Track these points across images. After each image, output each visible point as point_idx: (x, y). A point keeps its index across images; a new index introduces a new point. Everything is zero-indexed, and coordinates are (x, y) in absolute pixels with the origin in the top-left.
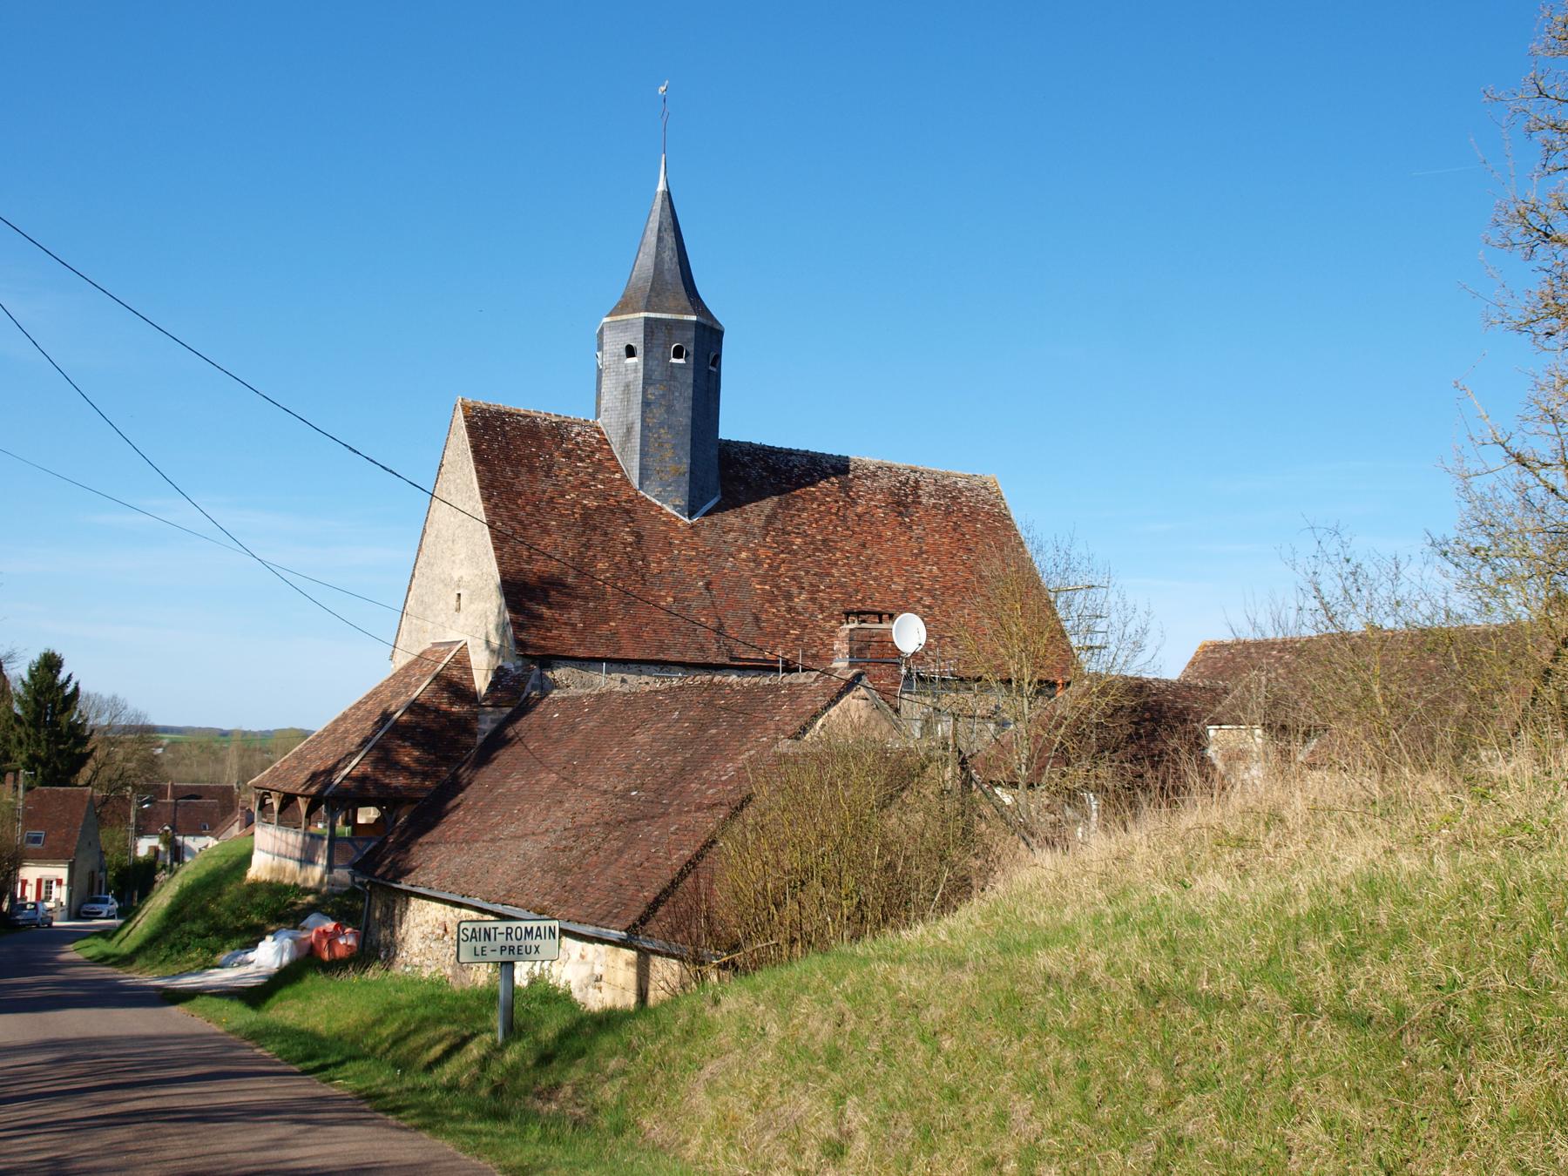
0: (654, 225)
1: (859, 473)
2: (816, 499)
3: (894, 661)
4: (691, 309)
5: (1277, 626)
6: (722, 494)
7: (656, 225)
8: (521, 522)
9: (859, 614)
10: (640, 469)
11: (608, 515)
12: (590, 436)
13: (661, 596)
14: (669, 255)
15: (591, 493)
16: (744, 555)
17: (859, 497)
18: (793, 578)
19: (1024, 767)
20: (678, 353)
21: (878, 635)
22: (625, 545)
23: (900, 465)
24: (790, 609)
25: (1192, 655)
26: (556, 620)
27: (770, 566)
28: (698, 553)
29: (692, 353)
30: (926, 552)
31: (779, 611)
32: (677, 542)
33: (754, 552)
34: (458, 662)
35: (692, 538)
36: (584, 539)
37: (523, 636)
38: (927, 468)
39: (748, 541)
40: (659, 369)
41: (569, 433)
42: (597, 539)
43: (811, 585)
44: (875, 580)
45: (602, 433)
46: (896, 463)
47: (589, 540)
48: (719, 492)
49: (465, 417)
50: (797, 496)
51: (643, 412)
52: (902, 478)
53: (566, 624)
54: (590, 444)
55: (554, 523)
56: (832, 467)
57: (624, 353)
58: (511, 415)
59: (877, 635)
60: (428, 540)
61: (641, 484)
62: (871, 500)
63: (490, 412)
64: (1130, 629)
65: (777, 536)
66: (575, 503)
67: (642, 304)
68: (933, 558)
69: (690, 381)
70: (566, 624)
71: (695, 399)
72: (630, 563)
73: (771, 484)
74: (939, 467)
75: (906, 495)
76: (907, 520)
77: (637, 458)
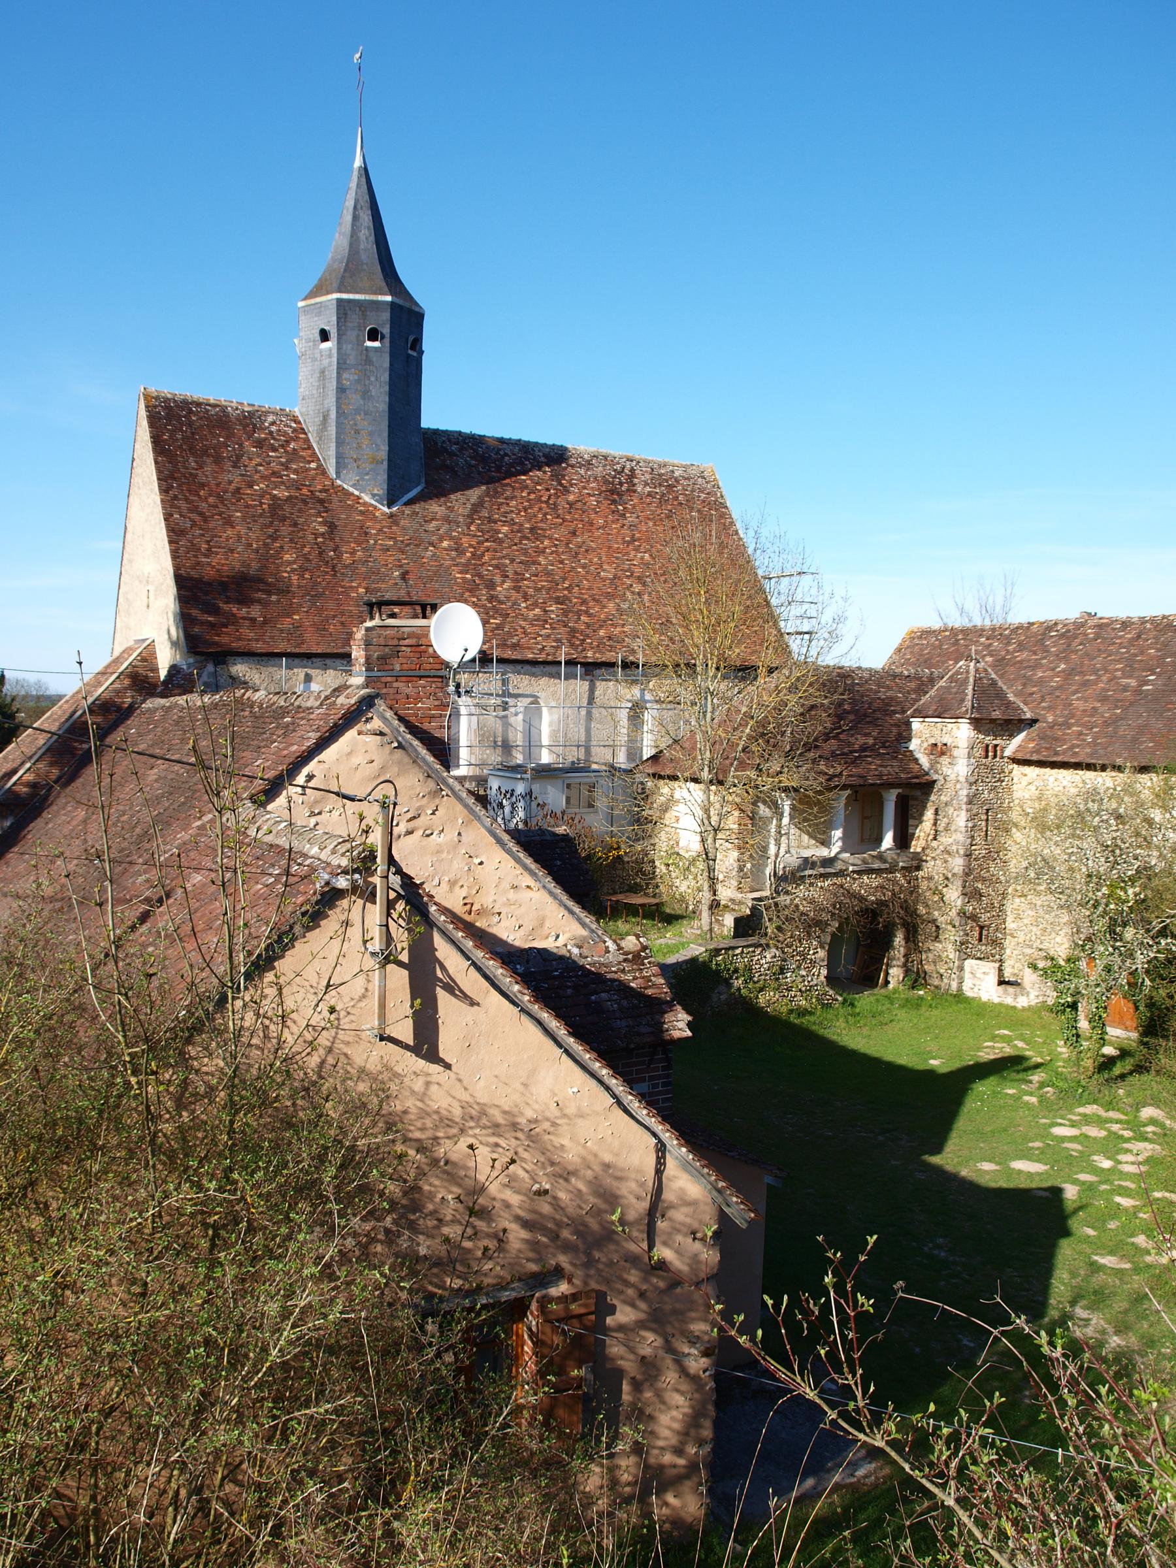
0: (350, 203)
4: (386, 289)
5: (984, 612)
6: (426, 482)
7: (352, 203)
8: (201, 514)
9: (381, 604)
10: (337, 458)
11: (300, 505)
12: (287, 426)
13: (351, 587)
15: (282, 483)
16: (445, 544)
17: (572, 485)
18: (497, 567)
19: (706, 769)
20: (373, 335)
22: (316, 536)
24: (491, 599)
25: (899, 641)
27: (473, 554)
28: (396, 542)
29: (388, 336)
30: (639, 540)
31: (479, 600)
33: (457, 540)
34: (144, 660)
35: (390, 527)
36: (271, 530)
38: (643, 457)
39: (451, 530)
40: (354, 353)
42: (285, 530)
43: (516, 573)
44: (583, 568)
45: (300, 423)
46: (612, 452)
47: (276, 531)
48: (423, 480)
49: (147, 407)
50: (506, 485)
51: (338, 399)
52: (618, 467)
54: (285, 434)
55: (239, 514)
57: (318, 338)
58: (199, 404)
59: (410, 635)
61: (338, 473)
62: (584, 488)
63: (175, 401)
65: (482, 524)
66: (263, 494)
67: (335, 285)
69: (387, 364)
72: (320, 553)
73: (479, 473)
75: (621, 484)
77: (333, 445)
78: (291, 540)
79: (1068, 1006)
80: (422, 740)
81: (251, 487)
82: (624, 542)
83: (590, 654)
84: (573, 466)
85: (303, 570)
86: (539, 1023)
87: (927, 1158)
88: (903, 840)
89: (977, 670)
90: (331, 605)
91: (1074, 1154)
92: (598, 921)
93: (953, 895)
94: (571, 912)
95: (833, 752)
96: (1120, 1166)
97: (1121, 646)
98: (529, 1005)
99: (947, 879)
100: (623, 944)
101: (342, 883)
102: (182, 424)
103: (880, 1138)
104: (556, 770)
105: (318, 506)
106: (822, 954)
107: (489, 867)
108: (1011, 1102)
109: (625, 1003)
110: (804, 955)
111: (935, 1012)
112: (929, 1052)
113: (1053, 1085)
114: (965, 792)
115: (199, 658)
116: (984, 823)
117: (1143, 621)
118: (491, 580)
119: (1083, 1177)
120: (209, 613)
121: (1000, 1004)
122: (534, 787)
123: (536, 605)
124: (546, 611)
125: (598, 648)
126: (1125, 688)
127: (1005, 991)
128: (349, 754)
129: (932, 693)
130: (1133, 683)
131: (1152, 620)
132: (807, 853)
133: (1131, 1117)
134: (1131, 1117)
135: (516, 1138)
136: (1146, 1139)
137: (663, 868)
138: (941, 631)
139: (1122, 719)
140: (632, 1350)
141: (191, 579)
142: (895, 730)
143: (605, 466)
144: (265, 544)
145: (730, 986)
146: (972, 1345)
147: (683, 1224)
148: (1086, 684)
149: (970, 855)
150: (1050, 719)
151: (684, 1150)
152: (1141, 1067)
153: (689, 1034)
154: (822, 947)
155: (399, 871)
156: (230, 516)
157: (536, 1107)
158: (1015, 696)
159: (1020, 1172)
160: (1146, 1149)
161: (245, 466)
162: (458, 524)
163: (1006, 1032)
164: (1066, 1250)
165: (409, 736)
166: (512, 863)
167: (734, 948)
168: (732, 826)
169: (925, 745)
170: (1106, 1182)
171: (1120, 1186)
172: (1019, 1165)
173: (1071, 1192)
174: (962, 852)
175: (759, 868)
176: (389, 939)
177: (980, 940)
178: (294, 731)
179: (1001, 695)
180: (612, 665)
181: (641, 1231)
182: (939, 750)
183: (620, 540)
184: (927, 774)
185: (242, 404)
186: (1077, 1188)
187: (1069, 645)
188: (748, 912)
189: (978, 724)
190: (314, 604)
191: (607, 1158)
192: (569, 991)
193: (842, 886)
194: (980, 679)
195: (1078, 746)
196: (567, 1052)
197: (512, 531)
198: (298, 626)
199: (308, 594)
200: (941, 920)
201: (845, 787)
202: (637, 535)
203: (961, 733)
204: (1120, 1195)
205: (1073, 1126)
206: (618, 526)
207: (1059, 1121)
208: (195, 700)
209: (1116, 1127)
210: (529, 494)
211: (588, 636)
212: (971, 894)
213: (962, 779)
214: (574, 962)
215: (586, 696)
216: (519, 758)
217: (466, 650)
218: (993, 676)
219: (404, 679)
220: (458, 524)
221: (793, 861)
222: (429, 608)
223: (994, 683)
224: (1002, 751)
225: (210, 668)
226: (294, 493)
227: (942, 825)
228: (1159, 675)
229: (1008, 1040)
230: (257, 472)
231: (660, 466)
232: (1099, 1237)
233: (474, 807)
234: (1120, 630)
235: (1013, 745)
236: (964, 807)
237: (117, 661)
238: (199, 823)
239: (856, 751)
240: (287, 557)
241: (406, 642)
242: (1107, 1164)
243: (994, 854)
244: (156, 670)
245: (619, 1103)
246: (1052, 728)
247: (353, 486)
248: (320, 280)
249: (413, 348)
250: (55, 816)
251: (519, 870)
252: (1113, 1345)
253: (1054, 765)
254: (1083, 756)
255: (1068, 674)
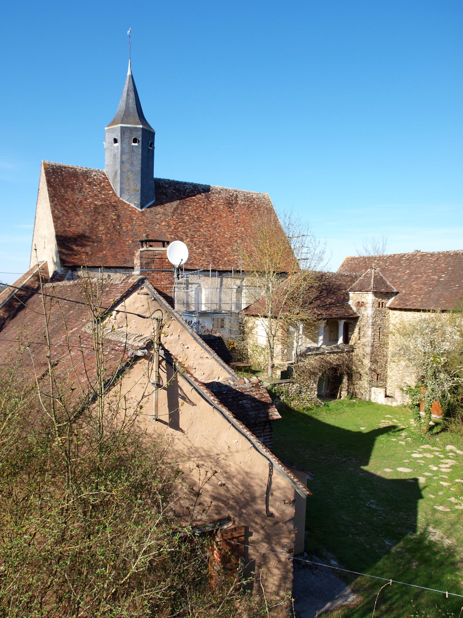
0: (126, 89)
1: (213, 191)
2: (195, 201)
3: (170, 270)
4: (140, 122)
5: (375, 251)
6: (156, 199)
7: (127, 89)
8: (66, 211)
11: (106, 208)
13: (126, 240)
14: (132, 101)
15: (99, 199)
16: (163, 223)
17: (213, 201)
18: (184, 233)
19: (270, 312)
20: (135, 141)
21: (159, 254)
22: (112, 220)
23: (231, 189)
25: (343, 262)
26: (79, 251)
27: (175, 228)
29: (141, 141)
30: (240, 222)
32: (135, 218)
33: (168, 222)
34: (43, 269)
35: (141, 217)
36: (94, 218)
37: (64, 257)
38: (241, 190)
39: (165, 218)
41: (91, 175)
42: (100, 218)
43: (191, 235)
45: (105, 175)
46: (229, 188)
47: (96, 218)
48: (155, 198)
49: (45, 168)
50: (187, 200)
51: (121, 166)
52: (231, 194)
53: (84, 253)
55: (81, 211)
56: (202, 189)
57: (113, 142)
58: (65, 168)
59: (159, 254)
60: (37, 220)
61: (121, 195)
62: (218, 202)
63: (56, 166)
64: (317, 251)
66: (91, 203)
67: (120, 121)
68: (242, 225)
69: (140, 152)
70: (84, 253)
71: (142, 160)
72: (114, 227)
73: (177, 196)
74: (246, 190)
75: (232, 200)
76: (232, 210)
77: (119, 184)
78: (102, 222)
79: (416, 405)
80: (164, 297)
81: (86, 200)
82: (234, 223)
83: (221, 267)
84: (213, 193)
85: (107, 233)
86: (222, 413)
87: (362, 467)
88: (346, 340)
89: (375, 273)
90: (118, 247)
91: (422, 464)
92: (235, 371)
93: (367, 362)
94: (224, 368)
95: (319, 305)
96: (440, 469)
97: (431, 263)
98: (217, 405)
99: (364, 355)
100: (251, 380)
101: (140, 353)
102: (59, 175)
103: (344, 459)
104: (208, 313)
105: (113, 208)
106: (315, 386)
107: (191, 349)
108: (394, 444)
109: (253, 404)
110: (308, 386)
111: (361, 408)
112: (360, 424)
113: (410, 437)
114: (371, 321)
115: (65, 268)
116: (378, 333)
117: (439, 253)
118: (182, 238)
119: (427, 474)
120: (70, 251)
121: (386, 405)
122: (200, 320)
123: (199, 248)
124: (203, 250)
125: (224, 265)
126: (433, 280)
127: (388, 400)
128: (134, 302)
129: (357, 282)
130: (436, 277)
131: (443, 253)
132: (309, 346)
133: (443, 449)
134: (443, 449)
135: (211, 462)
136: (449, 458)
137: (251, 352)
138: (359, 258)
139: (432, 292)
140: (257, 551)
141: (62, 237)
142: (342, 297)
143: (226, 193)
144: (92, 223)
145: (280, 399)
146: (390, 544)
147: (278, 497)
148: (417, 278)
149: (373, 346)
150: (404, 292)
151: (280, 466)
152: (445, 429)
153: (280, 417)
154: (315, 383)
155: (163, 349)
156: (78, 212)
157: (219, 448)
158: (390, 283)
159: (401, 472)
160: (451, 462)
161: (84, 192)
162: (168, 216)
163: (389, 416)
164: (422, 505)
165: (158, 295)
166: (200, 348)
167: (281, 383)
168: (279, 335)
169: (355, 303)
170: (436, 476)
171: (442, 477)
172: (400, 469)
173: (422, 480)
174: (370, 345)
175: (290, 353)
176: (159, 377)
177: (377, 380)
178: (111, 293)
179: (384, 283)
180: (231, 272)
181: (262, 500)
182: (360, 304)
183: (232, 223)
184: (355, 314)
185: (82, 168)
186: (425, 478)
187: (410, 263)
188: (286, 369)
189: (376, 294)
190: (111, 247)
191: (247, 470)
192: (230, 400)
193: (323, 359)
194: (376, 276)
195: (415, 302)
196: (233, 425)
197: (190, 219)
198: (105, 256)
199: (109, 243)
200: (362, 372)
201: (324, 319)
202: (239, 221)
203: (369, 298)
204: (442, 481)
205: (420, 453)
206: (231, 217)
207: (415, 451)
208: (65, 283)
209: (437, 454)
210: (196, 204)
211: (220, 260)
212: (374, 361)
213: (370, 316)
214: (231, 387)
215: (219, 284)
216: (193, 308)
217: (182, 260)
218: (381, 275)
219: (156, 272)
220: (168, 216)
221: (303, 348)
222: (166, 243)
223: (381, 278)
224: (385, 305)
225: (70, 272)
226: (103, 203)
227: (362, 334)
228: (446, 274)
229: (390, 419)
230: (88, 194)
231: (247, 193)
232: (436, 498)
233: (185, 325)
234: (430, 257)
235: (390, 302)
236: (371, 327)
237: (32, 270)
238: (71, 331)
239: (327, 305)
240: (101, 228)
241: (157, 257)
242: (435, 468)
243: (384, 345)
244: (47, 273)
245: (254, 447)
246: (404, 295)
247: (127, 200)
248: (114, 119)
249: (151, 146)
250: (8, 331)
251: (203, 351)
252: (447, 543)
253: (406, 310)
254: (417, 307)
255: (410, 274)
